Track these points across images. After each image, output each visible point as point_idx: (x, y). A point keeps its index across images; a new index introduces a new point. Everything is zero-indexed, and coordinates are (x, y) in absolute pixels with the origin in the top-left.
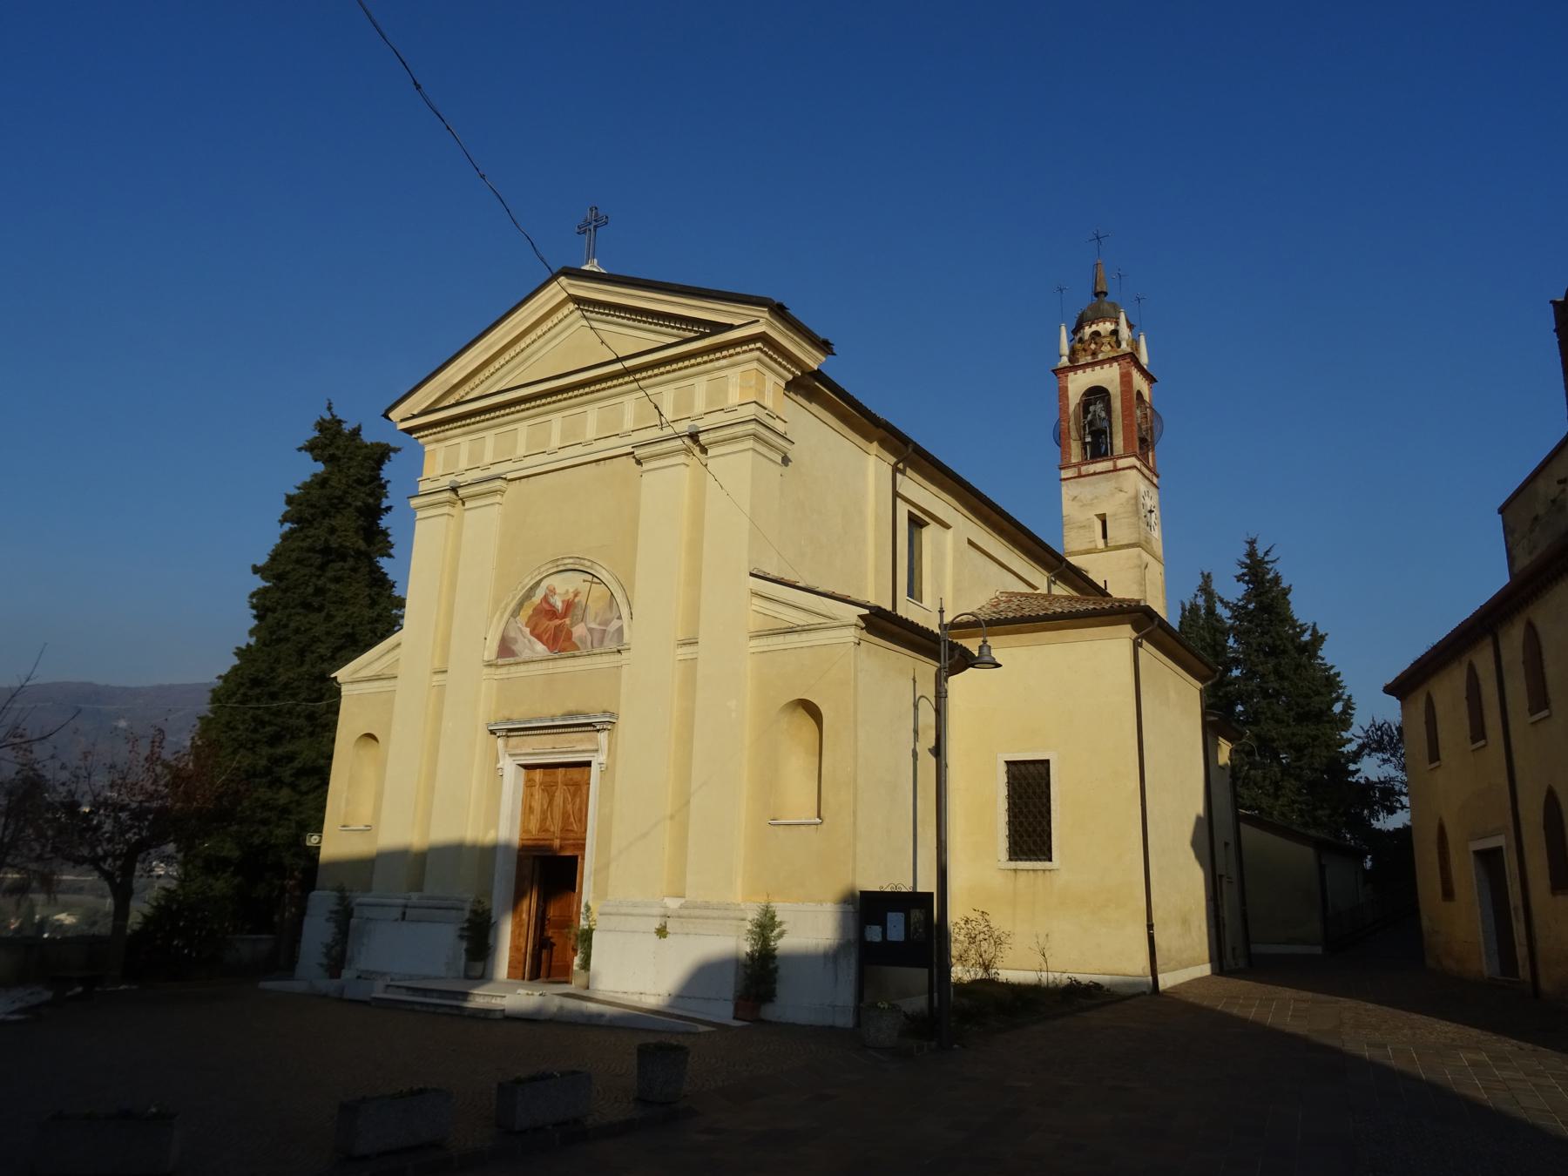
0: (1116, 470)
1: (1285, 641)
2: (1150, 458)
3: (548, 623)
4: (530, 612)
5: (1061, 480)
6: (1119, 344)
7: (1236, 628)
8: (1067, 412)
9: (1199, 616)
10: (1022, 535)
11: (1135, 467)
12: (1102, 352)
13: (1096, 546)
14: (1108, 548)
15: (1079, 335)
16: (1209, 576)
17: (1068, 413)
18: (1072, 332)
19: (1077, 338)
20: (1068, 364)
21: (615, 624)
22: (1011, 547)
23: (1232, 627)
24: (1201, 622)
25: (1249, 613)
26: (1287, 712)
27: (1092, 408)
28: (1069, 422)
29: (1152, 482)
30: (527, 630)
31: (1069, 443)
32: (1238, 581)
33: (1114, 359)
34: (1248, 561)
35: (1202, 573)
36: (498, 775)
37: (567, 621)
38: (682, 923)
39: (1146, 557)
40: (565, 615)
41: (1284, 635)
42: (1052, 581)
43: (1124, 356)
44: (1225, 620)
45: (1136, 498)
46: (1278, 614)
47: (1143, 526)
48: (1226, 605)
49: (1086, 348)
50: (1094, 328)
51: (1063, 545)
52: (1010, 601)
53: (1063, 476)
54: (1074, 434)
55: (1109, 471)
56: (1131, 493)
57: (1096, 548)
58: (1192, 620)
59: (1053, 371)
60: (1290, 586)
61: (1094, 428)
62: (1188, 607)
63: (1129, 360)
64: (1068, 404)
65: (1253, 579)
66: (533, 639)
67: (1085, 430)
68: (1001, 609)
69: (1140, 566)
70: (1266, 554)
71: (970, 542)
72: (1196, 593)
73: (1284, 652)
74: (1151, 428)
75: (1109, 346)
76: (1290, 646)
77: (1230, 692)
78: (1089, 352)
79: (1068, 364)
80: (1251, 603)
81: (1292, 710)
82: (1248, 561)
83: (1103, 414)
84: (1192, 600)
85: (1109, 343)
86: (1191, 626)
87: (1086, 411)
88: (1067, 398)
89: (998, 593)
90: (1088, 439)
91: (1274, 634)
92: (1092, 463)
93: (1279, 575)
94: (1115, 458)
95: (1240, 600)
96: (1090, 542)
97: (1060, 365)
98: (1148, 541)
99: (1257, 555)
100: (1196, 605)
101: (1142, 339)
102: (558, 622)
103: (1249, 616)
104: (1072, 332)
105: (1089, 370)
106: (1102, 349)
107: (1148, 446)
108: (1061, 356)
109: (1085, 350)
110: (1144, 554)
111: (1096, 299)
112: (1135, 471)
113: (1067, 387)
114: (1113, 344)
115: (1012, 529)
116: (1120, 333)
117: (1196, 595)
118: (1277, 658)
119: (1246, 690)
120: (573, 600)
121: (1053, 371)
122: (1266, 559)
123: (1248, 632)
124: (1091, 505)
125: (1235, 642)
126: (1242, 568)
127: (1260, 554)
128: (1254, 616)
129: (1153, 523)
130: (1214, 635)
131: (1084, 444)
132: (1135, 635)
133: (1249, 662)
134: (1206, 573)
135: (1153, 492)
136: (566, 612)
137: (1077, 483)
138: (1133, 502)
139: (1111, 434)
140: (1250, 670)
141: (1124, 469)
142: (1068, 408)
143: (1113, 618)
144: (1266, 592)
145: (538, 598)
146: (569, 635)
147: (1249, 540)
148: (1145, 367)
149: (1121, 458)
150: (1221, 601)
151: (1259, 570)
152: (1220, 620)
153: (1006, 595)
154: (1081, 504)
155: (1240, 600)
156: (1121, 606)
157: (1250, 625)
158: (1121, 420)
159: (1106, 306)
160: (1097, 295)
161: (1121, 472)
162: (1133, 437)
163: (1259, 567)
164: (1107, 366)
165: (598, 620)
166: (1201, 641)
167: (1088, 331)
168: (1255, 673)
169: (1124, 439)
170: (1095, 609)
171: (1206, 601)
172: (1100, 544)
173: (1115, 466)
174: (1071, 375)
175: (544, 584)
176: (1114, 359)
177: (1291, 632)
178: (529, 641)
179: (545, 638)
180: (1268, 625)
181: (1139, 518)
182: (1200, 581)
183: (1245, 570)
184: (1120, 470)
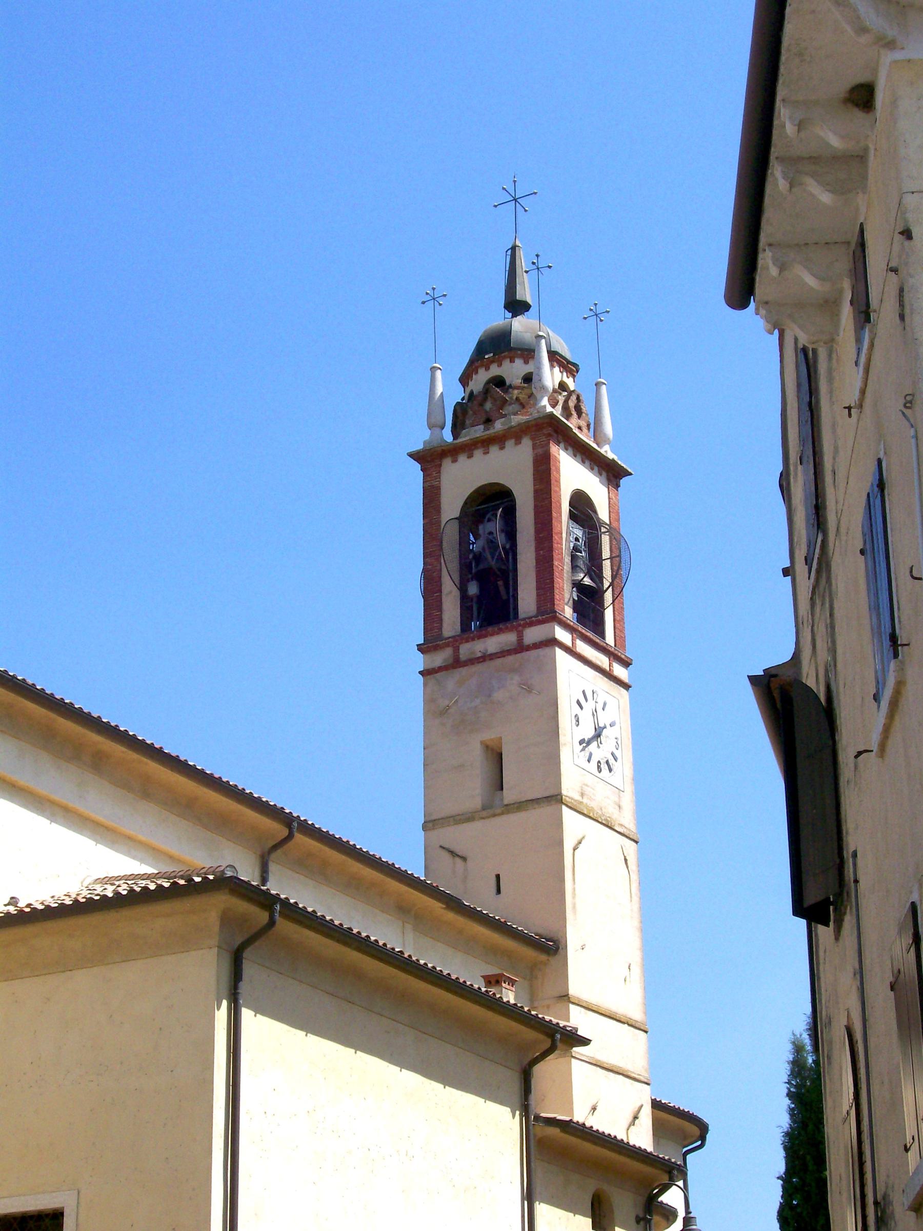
0: (520, 648)
50: (495, 371)
61: (481, 567)
92: (480, 637)
161: (534, 653)
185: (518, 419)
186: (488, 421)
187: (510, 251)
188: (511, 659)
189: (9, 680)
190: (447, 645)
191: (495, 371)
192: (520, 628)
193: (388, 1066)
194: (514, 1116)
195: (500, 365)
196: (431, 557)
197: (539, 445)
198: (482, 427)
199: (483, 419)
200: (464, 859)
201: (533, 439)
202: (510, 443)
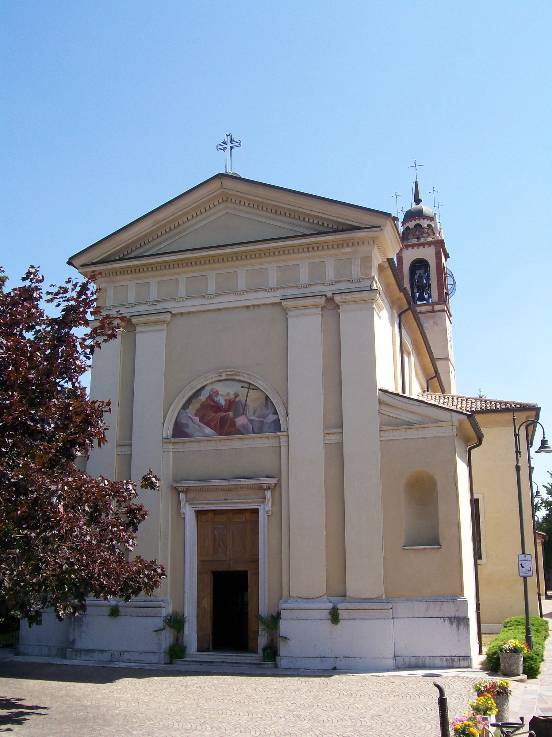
0: (433, 311)
3: (213, 414)
4: (198, 406)
21: (271, 418)
30: (197, 419)
36: (180, 517)
37: (231, 414)
38: (349, 613)
40: (228, 409)
50: (418, 222)
66: (202, 425)
102: (223, 414)
105: (415, 248)
120: (234, 400)
136: (229, 407)
145: (204, 397)
146: (233, 424)
149: (437, 304)
165: (257, 414)
175: (208, 389)
178: (199, 426)
179: (213, 424)
184: (436, 312)
185: (429, 239)
186: (418, 238)
187: (415, 183)
188: (430, 314)
191: (418, 222)
193: (532, 458)
194: (24, 723)
195: (419, 220)
198: (416, 240)
199: (417, 237)
201: (435, 246)
202: (427, 246)
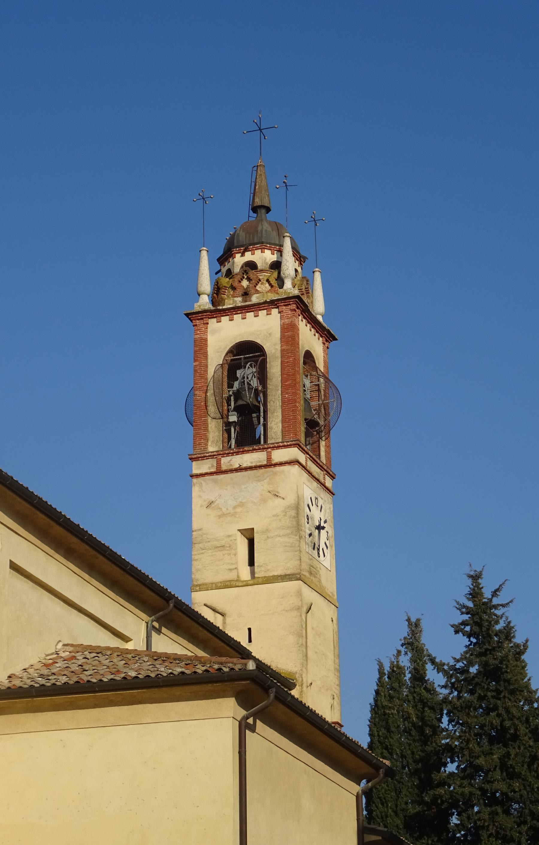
0: (270, 465)
1: (517, 722)
2: (323, 449)
5: (192, 476)
6: (281, 282)
7: (451, 702)
8: (204, 376)
9: (401, 683)
10: (101, 557)
11: (297, 462)
12: (257, 292)
13: (238, 576)
14: (255, 580)
15: (227, 266)
16: (417, 624)
17: (207, 379)
18: (218, 260)
19: (224, 270)
20: (209, 306)
22: (86, 576)
23: (445, 700)
24: (405, 692)
25: (469, 681)
26: (519, 825)
27: (239, 373)
28: (206, 392)
29: (323, 485)
31: (206, 424)
32: (456, 632)
33: (274, 304)
34: (470, 604)
35: (409, 620)
39: (309, 595)
41: (514, 711)
42: (154, 627)
43: (287, 300)
44: (438, 689)
45: (297, 507)
46: (508, 681)
47: (306, 548)
48: (439, 667)
49: (236, 284)
50: (248, 257)
51: (190, 573)
52: (74, 657)
53: (195, 471)
54: (212, 409)
55: (260, 467)
56: (291, 499)
57: (238, 580)
58: (392, 688)
59: (187, 315)
60: (527, 641)
61: (240, 402)
62: (387, 668)
63: (294, 306)
64: (207, 366)
65: (476, 629)
67: (229, 405)
68: (53, 671)
69: (299, 609)
70: (495, 593)
71: (14, 567)
72: (400, 648)
73: (515, 737)
74: (326, 407)
75: (267, 285)
76: (522, 729)
77: (441, 796)
78: (239, 292)
79: (209, 306)
80: (473, 666)
81: (525, 823)
82: (470, 604)
83: (255, 383)
84: (393, 660)
85: (268, 281)
86: (391, 697)
87: (232, 377)
88: (206, 357)
89: (60, 646)
90: (233, 418)
91: (501, 711)
92: (237, 453)
93: (512, 625)
94: (269, 448)
95: (458, 661)
96: (231, 570)
97: (197, 308)
98: (313, 571)
99: (482, 594)
100: (399, 667)
101: (318, 277)
103: (470, 684)
104: (218, 260)
105: (237, 317)
106: (258, 288)
107: (319, 433)
108: (199, 295)
109: (233, 288)
110: (306, 590)
111: (255, 215)
112: (296, 469)
113: (206, 340)
114: (273, 282)
115: (83, 548)
116: (284, 267)
117: (399, 652)
118: (506, 745)
119: (462, 794)
121: (187, 315)
122: (495, 601)
123: (467, 707)
124: (234, 515)
125: (450, 721)
126: (462, 613)
127: (487, 593)
128: (477, 684)
129: (322, 546)
130: (423, 712)
131: (228, 425)
132: (241, 713)
133: (466, 752)
134: (413, 620)
135: (325, 499)
137: (215, 481)
138: (293, 513)
139: (265, 412)
140: (471, 765)
141: (281, 464)
142: (206, 371)
143: (209, 687)
144: (494, 649)
147: (472, 573)
148: (320, 318)
149: (278, 447)
150: (433, 661)
151: (485, 617)
152: (431, 690)
153: (71, 649)
154: (220, 513)
155: (458, 661)
156: (220, 669)
157: (472, 698)
158: (280, 392)
159: (266, 226)
160: (255, 209)
161: (278, 469)
162: (295, 418)
163: (485, 613)
164: (263, 313)
166: (404, 720)
167: (239, 260)
168: (479, 768)
169: (283, 421)
170: (183, 673)
171: (412, 661)
172: (245, 573)
173: (269, 458)
174: (213, 322)
176: (274, 304)
177: (526, 708)
180: (493, 697)
181: (301, 537)
182: (404, 631)
183: (466, 617)
184: (275, 465)
189: (442, 716)
190: (212, 457)
192: (270, 450)
196: (200, 391)
197: (286, 317)
200: (223, 615)
